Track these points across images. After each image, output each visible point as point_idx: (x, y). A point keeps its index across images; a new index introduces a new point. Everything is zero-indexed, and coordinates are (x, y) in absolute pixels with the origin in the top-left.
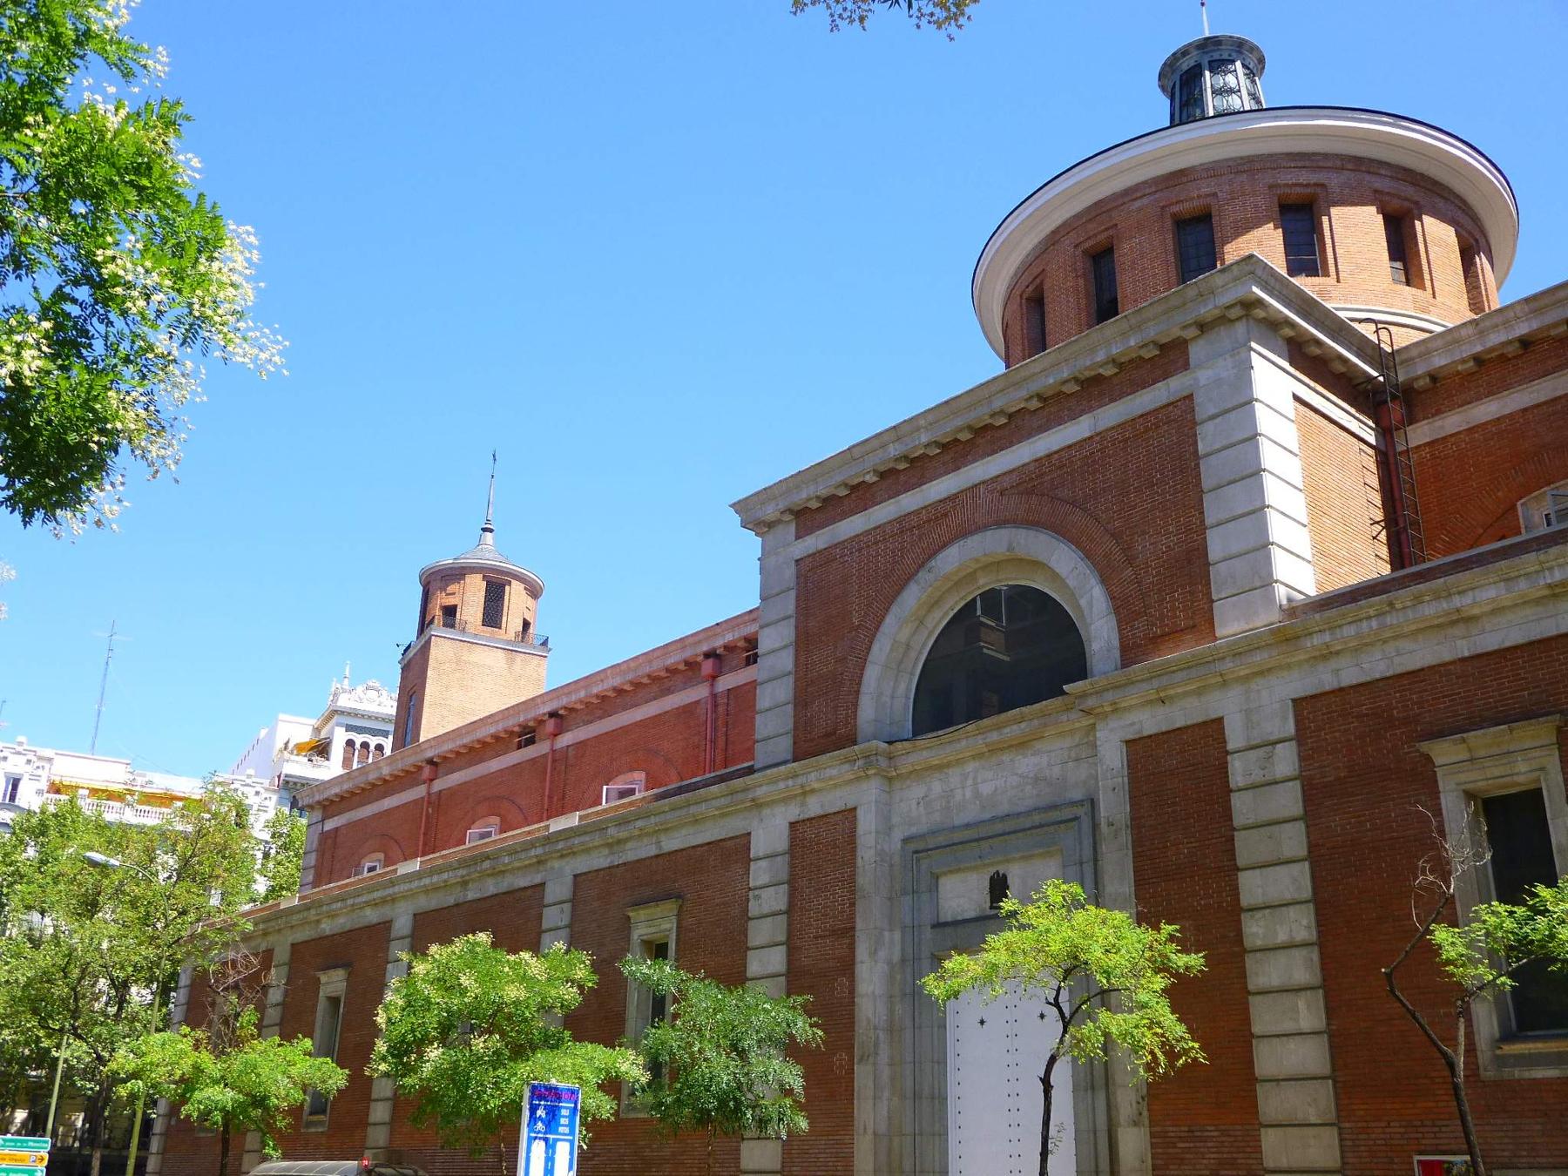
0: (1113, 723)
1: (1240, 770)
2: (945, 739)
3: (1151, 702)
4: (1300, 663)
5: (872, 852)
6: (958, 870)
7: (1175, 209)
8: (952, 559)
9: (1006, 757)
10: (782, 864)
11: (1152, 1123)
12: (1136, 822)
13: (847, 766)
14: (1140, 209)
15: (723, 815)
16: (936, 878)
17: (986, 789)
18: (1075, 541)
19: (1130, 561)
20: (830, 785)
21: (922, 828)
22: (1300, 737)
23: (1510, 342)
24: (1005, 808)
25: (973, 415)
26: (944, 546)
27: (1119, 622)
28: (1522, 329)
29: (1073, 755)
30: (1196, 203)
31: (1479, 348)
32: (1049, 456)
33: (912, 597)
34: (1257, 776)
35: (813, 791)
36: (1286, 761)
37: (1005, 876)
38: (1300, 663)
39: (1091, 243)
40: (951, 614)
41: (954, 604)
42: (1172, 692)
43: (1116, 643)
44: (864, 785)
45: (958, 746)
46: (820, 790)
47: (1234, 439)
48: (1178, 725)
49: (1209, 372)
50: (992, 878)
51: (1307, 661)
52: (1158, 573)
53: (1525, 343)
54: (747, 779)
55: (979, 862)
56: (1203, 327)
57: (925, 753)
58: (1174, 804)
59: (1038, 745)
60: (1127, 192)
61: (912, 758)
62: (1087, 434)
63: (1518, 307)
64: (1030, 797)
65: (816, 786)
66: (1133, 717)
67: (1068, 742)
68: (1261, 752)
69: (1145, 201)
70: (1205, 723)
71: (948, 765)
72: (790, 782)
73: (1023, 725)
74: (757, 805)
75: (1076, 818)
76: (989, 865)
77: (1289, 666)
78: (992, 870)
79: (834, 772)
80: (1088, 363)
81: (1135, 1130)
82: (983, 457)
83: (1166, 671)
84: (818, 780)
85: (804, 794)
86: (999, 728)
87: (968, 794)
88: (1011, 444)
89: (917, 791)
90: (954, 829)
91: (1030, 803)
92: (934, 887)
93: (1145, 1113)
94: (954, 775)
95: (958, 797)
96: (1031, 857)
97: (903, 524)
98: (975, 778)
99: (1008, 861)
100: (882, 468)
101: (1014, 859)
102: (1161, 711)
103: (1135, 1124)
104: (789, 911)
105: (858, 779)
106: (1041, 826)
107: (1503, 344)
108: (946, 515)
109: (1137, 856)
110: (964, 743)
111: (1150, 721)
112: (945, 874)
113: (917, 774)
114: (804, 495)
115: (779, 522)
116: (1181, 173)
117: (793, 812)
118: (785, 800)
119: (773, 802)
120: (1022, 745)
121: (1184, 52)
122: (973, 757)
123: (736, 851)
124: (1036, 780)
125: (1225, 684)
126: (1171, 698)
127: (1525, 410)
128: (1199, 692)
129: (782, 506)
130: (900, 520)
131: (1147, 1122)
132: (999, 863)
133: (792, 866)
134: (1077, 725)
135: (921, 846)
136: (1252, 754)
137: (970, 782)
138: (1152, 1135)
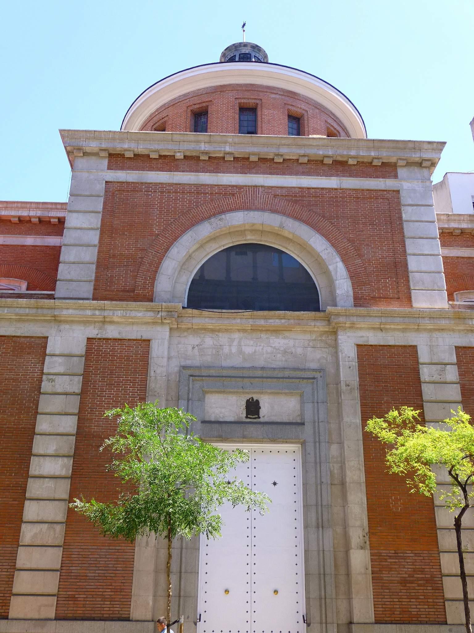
0: (350, 333)
1: (425, 373)
2: (226, 315)
3: (374, 329)
4: (460, 331)
5: (164, 369)
6: (224, 392)
7: (290, 107)
8: (237, 218)
9: (263, 335)
10: (79, 365)
11: (372, 548)
12: (362, 387)
13: (151, 314)
14: (275, 99)
15: (19, 320)
16: (205, 393)
17: (248, 350)
18: (326, 236)
19: (360, 256)
20: (125, 322)
21: (197, 362)
22: (459, 364)
23: (458, 229)
24: (261, 363)
25: (266, 150)
26: (231, 210)
27: (353, 284)
28: (464, 226)
29: (311, 344)
30: (299, 110)
31: (446, 226)
32: (309, 188)
33: (205, 230)
34: (436, 378)
35: (112, 322)
36: (452, 374)
37: (257, 402)
38: (460, 331)
39: (245, 101)
40: (223, 248)
41: (227, 243)
42: (388, 327)
43: (351, 293)
44: (159, 328)
45: (234, 321)
46: (118, 323)
47: (423, 219)
48: (390, 344)
49: (409, 185)
50: (248, 401)
51: (463, 330)
52: (376, 267)
53: (463, 232)
54: (46, 301)
55: (241, 390)
56: (409, 164)
57: (207, 320)
58: (386, 382)
59: (287, 334)
60: (268, 87)
61: (195, 321)
62: (335, 187)
63: (466, 217)
64: (279, 361)
65: (116, 319)
66: (360, 333)
67: (308, 337)
68: (439, 367)
69: (277, 96)
70: (405, 346)
71: (219, 331)
72: (97, 312)
73: (283, 321)
74: (57, 320)
75: (314, 378)
76: (248, 393)
77: (453, 330)
78: (248, 397)
79: (140, 314)
80: (345, 153)
81: (362, 551)
82: (264, 173)
83: (391, 315)
84: (123, 317)
85: (104, 322)
86: (265, 318)
87: (234, 350)
88: (284, 174)
89: (193, 340)
90: (223, 368)
91: (279, 364)
92: (202, 400)
93: (368, 542)
94: (223, 339)
95: (226, 350)
96: (278, 393)
97: (199, 190)
98: (239, 342)
99: (262, 393)
100: (188, 154)
101: (266, 393)
102: (380, 335)
103: (362, 548)
104: (83, 393)
105: (154, 323)
106: (289, 378)
107: (455, 229)
108: (233, 195)
109: (363, 405)
110: (239, 321)
111: (374, 338)
112: (212, 392)
113: (195, 331)
114: (126, 146)
115: (96, 154)
116: (294, 94)
117: (93, 332)
118: (86, 323)
119: (72, 322)
120: (276, 331)
121: (245, 45)
122: (239, 330)
123: (38, 347)
124: (285, 352)
125: (418, 330)
126: (386, 329)
127: (458, 257)
128: (404, 330)
129: (104, 146)
130: (197, 186)
131: (368, 547)
132: (254, 393)
133: (87, 366)
134: (316, 329)
135: (197, 373)
136: (434, 367)
137: (235, 343)
138: (372, 555)
